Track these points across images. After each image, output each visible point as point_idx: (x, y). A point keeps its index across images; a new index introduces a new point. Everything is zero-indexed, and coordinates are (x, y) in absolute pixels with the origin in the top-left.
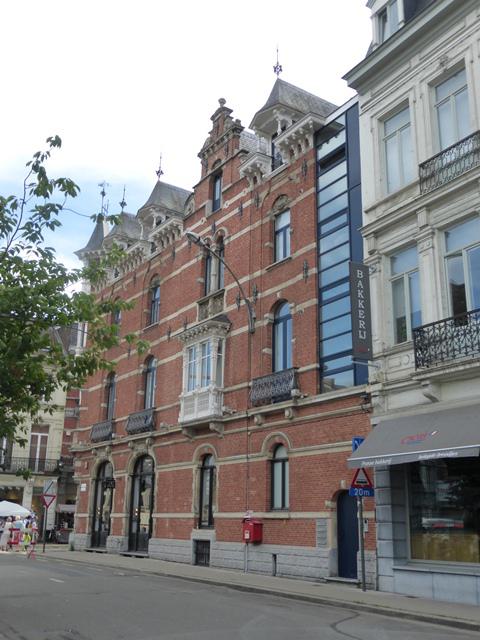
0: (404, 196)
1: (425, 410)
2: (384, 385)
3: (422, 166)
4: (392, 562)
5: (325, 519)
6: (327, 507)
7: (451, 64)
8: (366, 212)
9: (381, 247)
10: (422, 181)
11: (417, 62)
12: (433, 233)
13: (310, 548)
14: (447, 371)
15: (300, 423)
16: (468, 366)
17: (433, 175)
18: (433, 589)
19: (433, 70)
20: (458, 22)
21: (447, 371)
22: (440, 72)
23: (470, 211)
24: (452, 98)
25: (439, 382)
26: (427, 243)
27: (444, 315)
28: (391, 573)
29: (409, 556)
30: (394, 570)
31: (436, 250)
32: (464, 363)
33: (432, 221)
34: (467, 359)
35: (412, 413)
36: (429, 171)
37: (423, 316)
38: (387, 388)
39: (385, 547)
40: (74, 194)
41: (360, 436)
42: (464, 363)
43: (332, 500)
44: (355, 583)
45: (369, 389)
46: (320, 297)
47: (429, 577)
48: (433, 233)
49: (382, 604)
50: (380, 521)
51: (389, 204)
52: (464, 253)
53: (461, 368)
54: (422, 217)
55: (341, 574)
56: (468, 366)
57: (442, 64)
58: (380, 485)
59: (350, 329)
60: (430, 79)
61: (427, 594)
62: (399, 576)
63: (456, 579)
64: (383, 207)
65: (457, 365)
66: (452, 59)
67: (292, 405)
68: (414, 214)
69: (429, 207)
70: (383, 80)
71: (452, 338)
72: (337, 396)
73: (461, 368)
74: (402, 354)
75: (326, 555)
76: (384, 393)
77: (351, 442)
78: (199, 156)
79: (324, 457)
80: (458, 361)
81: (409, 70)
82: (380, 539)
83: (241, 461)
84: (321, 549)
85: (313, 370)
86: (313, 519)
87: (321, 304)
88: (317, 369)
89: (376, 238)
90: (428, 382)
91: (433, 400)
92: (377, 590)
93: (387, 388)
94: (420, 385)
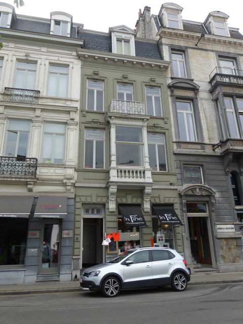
3: (6, 88)
12: (6, 118)
14: (5, 179)
16: (18, 180)
17: (10, 95)
20: (70, 51)
21: (5, 179)
22: (24, 58)
24: (26, 71)
27: (3, 154)
31: (5, 125)
32: (16, 178)
33: (42, 116)
34: (17, 176)
41: (66, 198)
42: (16, 178)
48: (6, 118)
53: (14, 179)
54: (38, 112)
56: (18, 180)
57: (26, 56)
60: (51, 61)
65: (12, 178)
68: (34, 109)
73: (24, 180)
78: (110, 29)
81: (40, 51)
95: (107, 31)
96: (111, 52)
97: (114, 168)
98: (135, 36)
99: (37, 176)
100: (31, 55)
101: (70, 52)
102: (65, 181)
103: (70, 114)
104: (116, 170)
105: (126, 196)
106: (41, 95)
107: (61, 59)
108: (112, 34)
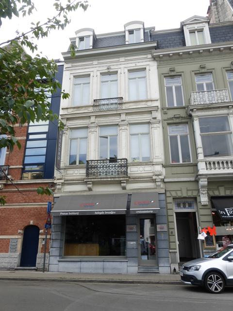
0: (84, 109)
1: (85, 194)
2: (65, 181)
3: (94, 100)
4: (58, 258)
5: (17, 239)
6: (20, 233)
7: (111, 70)
8: (62, 109)
9: (68, 125)
10: (94, 106)
11: (96, 63)
13: (5, 253)
15: (6, 192)
16: (112, 179)
17: (99, 106)
18: (81, 269)
19: (104, 69)
22: (107, 71)
23: (86, 125)
25: (94, 183)
26: (94, 129)
28: (57, 263)
29: (63, 255)
30: (59, 261)
32: (111, 178)
33: (96, 122)
35: (79, 194)
36: (96, 103)
37: (87, 157)
38: (65, 182)
39: (54, 251)
40: (23, 16)
42: (111, 178)
43: (22, 230)
44: (34, 269)
45: (55, 182)
46: (28, 137)
47: (79, 263)
49: (162, 279)
50: (52, 239)
51: (75, 109)
52: (109, 137)
53: (109, 179)
54: (93, 119)
55: (21, 265)
56: (112, 179)
57: (108, 69)
58: (55, 223)
59: (45, 154)
60: (101, 72)
61: (77, 271)
62: (62, 265)
63: (94, 263)
64: (72, 110)
65: (108, 178)
66: (112, 69)
67: (5, 183)
68: (89, 117)
69: (97, 116)
70: (76, 62)
71: (100, 167)
72: (35, 182)
73: (109, 179)
74: (75, 170)
75: (16, 256)
76: (63, 184)
77: (47, 203)
79: (21, 210)
80: (102, 177)
82: (52, 248)
83: (44, 206)
84: (11, 254)
85: (19, 168)
86: (8, 239)
87: (28, 140)
88: (22, 168)
89: (67, 120)
90: (91, 183)
91: (90, 189)
92: (48, 271)
93: (65, 182)
94: (86, 183)
95: (179, 26)
96: (185, 45)
97: (202, 161)
98: (208, 23)
99: (129, 175)
100: (112, 67)
101: (146, 56)
102: (154, 177)
103: (151, 113)
104: (205, 163)
105: (218, 188)
106: (124, 101)
107: (138, 64)
108: (184, 27)
